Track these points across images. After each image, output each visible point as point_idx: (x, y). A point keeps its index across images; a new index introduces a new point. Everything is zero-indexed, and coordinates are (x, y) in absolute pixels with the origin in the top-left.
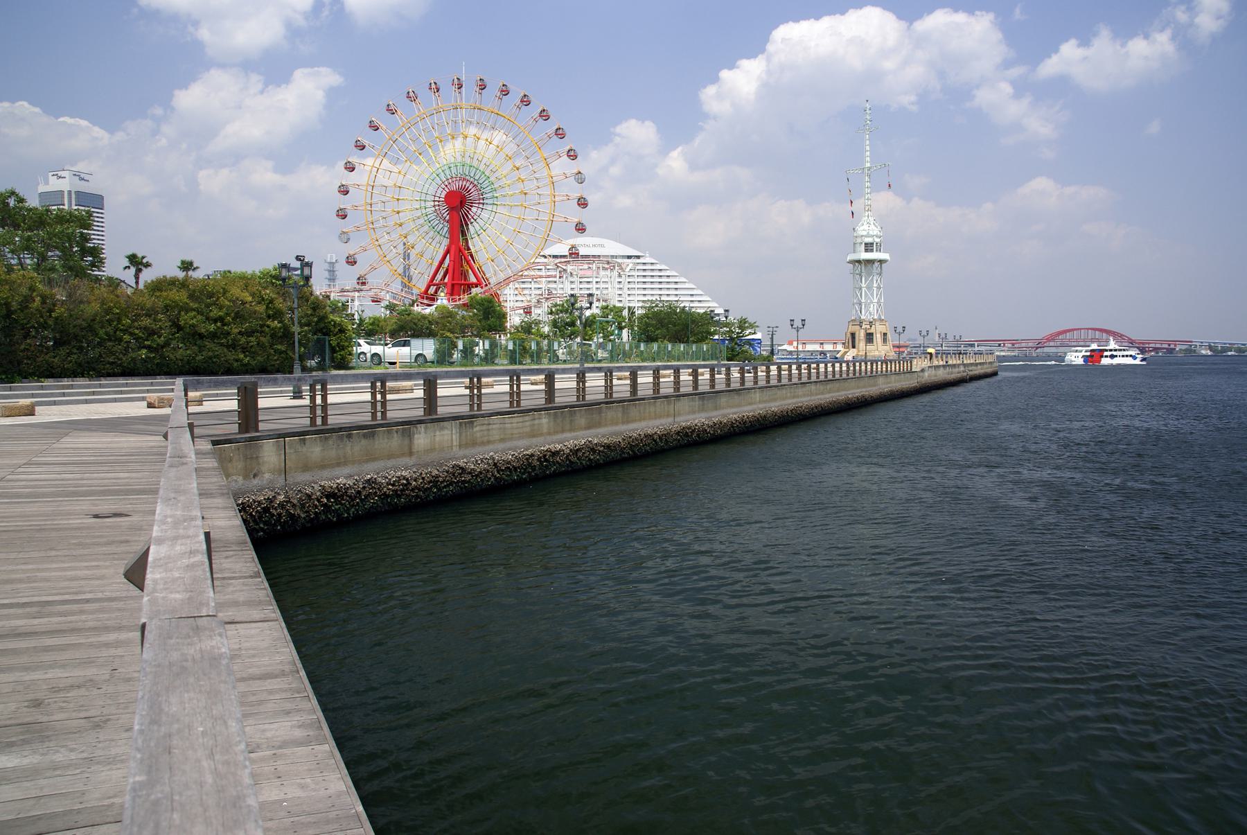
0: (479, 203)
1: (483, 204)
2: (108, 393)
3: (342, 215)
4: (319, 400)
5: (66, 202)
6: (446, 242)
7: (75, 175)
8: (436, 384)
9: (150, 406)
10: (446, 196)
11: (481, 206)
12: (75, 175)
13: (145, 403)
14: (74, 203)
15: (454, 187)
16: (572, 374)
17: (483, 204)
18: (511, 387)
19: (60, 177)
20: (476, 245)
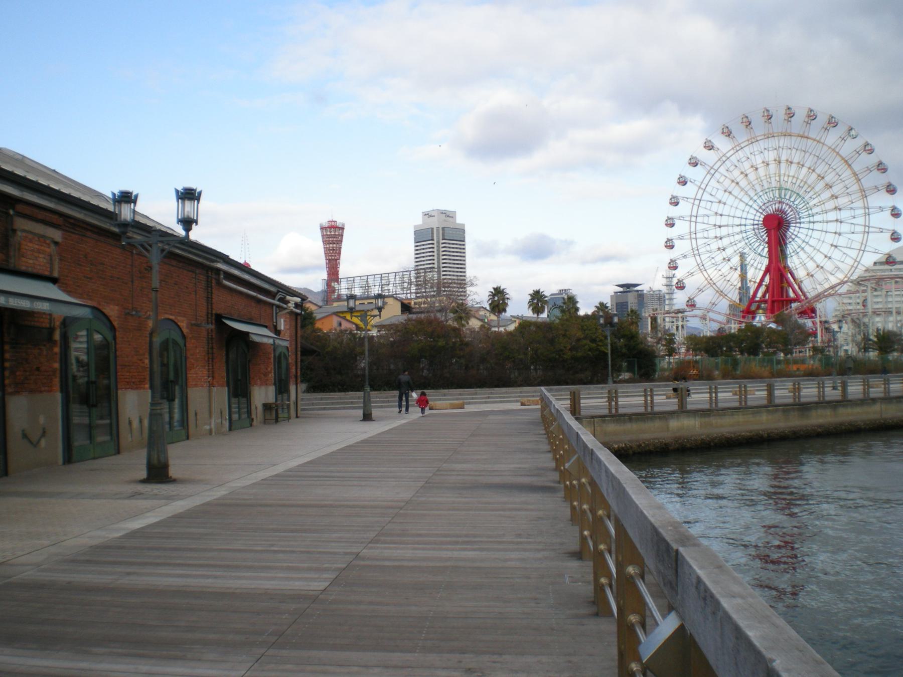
0: (796, 223)
1: (800, 228)
2: (497, 397)
3: (670, 245)
4: (649, 398)
5: (435, 238)
6: (766, 262)
7: (442, 213)
8: (774, 386)
9: (523, 404)
10: (764, 219)
11: (798, 225)
12: (442, 213)
13: (520, 404)
14: (441, 237)
15: (771, 210)
16: (622, 404)
17: (800, 223)
18: (716, 397)
19: (430, 216)
20: (793, 262)
